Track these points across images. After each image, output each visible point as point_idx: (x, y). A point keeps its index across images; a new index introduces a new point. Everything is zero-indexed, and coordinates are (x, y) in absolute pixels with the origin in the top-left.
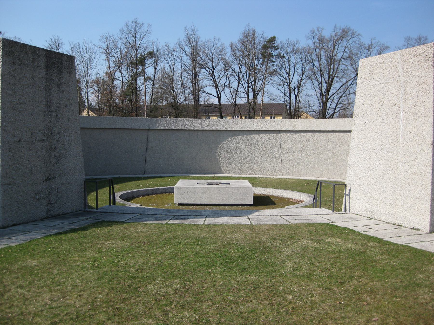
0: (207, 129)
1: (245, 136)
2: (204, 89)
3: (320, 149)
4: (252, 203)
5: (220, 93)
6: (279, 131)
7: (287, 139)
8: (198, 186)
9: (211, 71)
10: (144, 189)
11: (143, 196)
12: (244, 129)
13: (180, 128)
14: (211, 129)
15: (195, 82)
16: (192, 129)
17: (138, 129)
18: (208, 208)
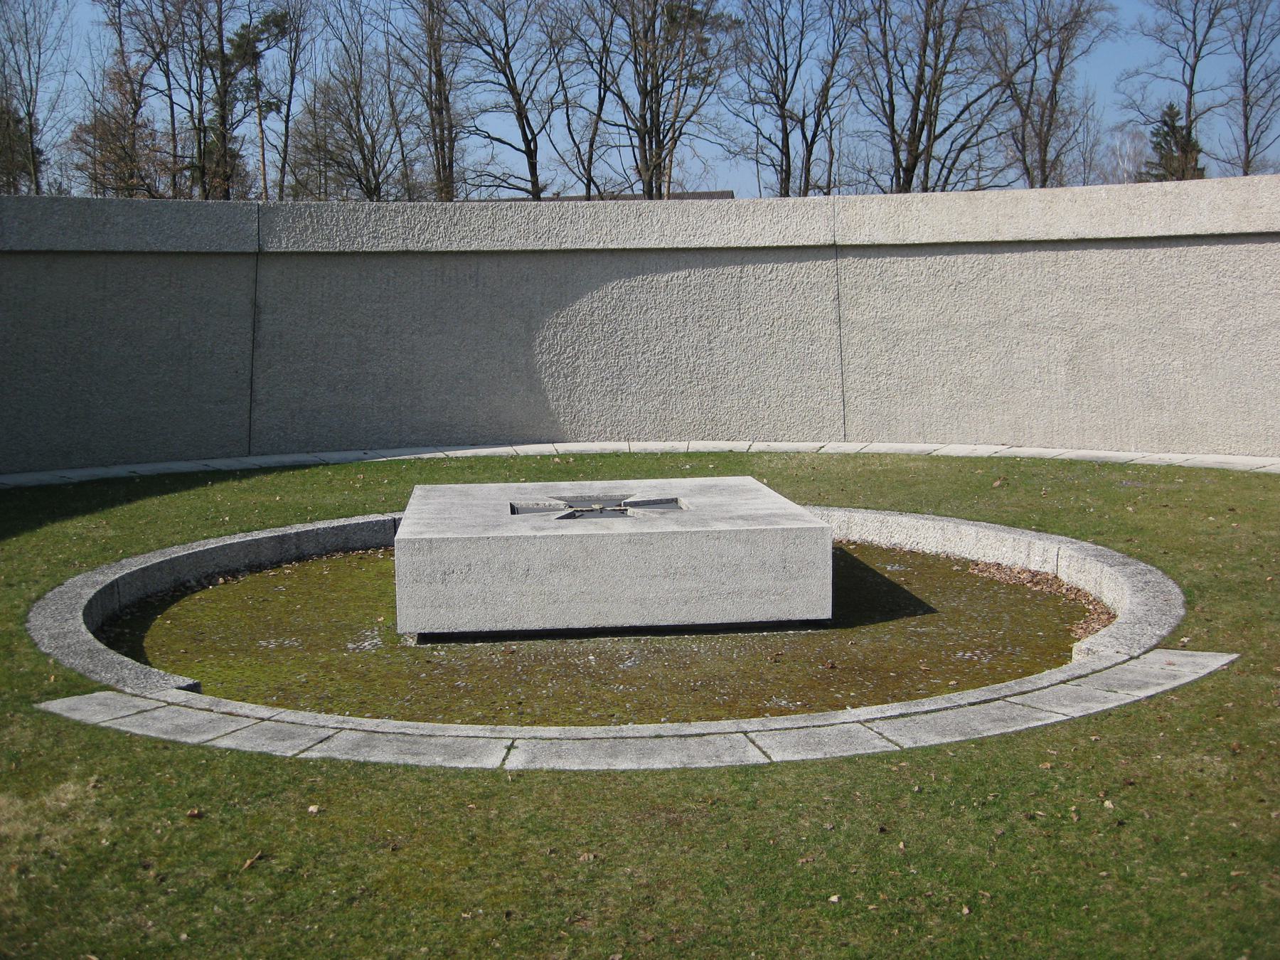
0: (519, 245)
1: (683, 274)
2: (477, 123)
3: (1016, 320)
4: (826, 613)
5: (534, 139)
6: (835, 250)
7: (870, 281)
8: (522, 527)
9: (499, 54)
10: (236, 539)
11: (233, 573)
12: (679, 243)
13: (398, 245)
14: (538, 246)
15: (439, 101)
16: (454, 248)
17: (207, 254)
18: (590, 643)
